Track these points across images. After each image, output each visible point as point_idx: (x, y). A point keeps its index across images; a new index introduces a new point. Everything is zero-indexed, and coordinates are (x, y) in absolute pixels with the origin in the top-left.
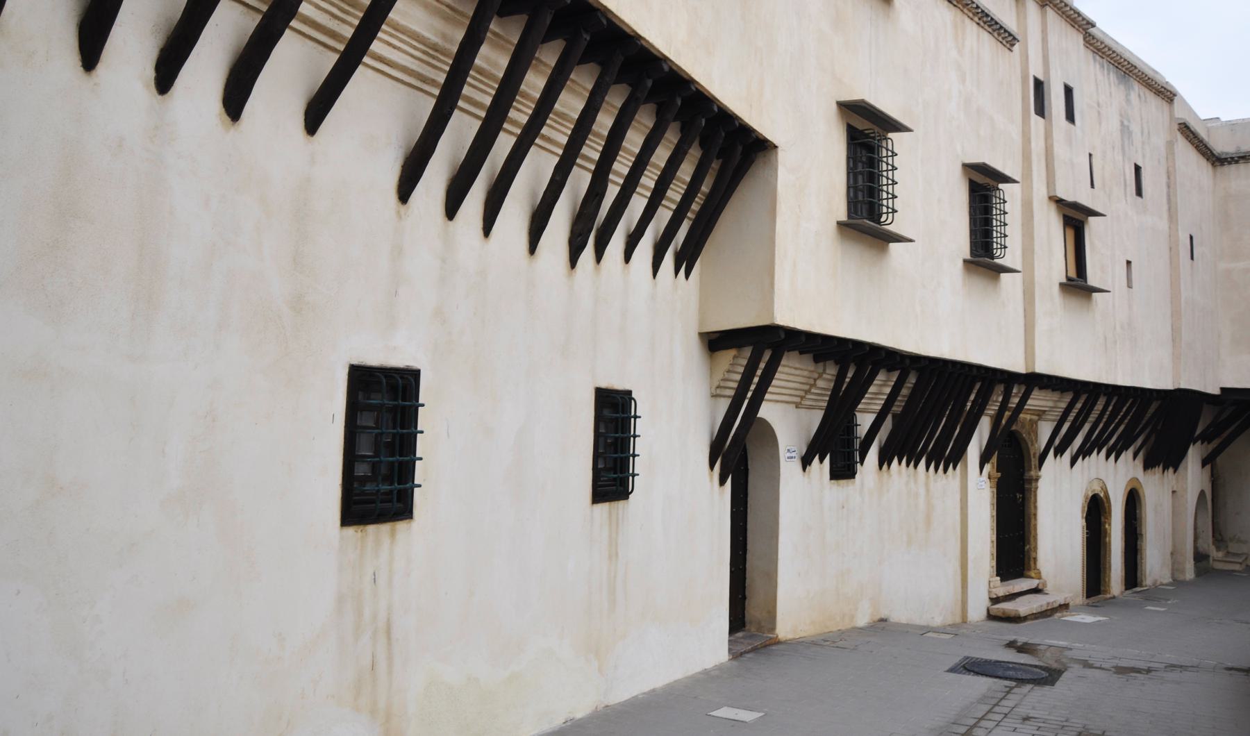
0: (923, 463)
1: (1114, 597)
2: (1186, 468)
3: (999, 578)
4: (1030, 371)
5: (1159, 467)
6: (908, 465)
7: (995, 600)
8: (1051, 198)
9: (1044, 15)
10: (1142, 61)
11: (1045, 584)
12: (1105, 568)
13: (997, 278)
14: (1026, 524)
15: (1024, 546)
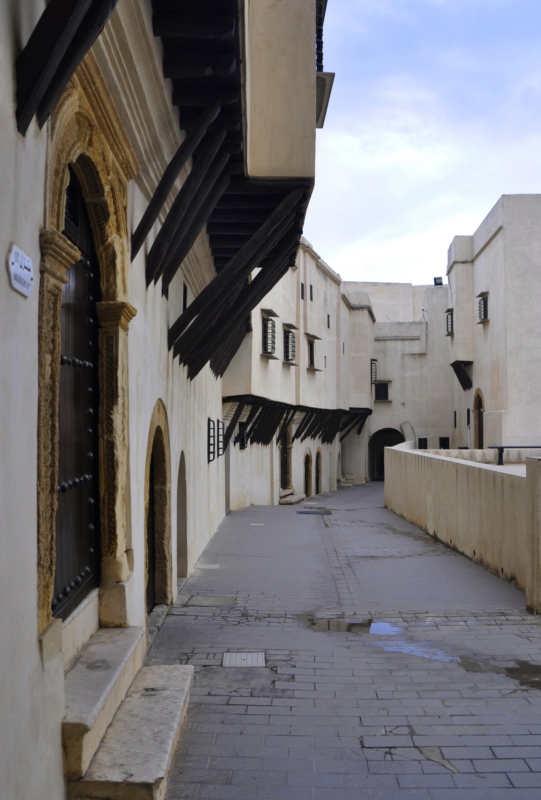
0: (261, 443)
1: (313, 498)
2: (335, 443)
3: (282, 489)
4: (298, 405)
6: (257, 444)
8: (305, 333)
9: (305, 256)
10: (332, 269)
12: (310, 485)
15: (287, 476)
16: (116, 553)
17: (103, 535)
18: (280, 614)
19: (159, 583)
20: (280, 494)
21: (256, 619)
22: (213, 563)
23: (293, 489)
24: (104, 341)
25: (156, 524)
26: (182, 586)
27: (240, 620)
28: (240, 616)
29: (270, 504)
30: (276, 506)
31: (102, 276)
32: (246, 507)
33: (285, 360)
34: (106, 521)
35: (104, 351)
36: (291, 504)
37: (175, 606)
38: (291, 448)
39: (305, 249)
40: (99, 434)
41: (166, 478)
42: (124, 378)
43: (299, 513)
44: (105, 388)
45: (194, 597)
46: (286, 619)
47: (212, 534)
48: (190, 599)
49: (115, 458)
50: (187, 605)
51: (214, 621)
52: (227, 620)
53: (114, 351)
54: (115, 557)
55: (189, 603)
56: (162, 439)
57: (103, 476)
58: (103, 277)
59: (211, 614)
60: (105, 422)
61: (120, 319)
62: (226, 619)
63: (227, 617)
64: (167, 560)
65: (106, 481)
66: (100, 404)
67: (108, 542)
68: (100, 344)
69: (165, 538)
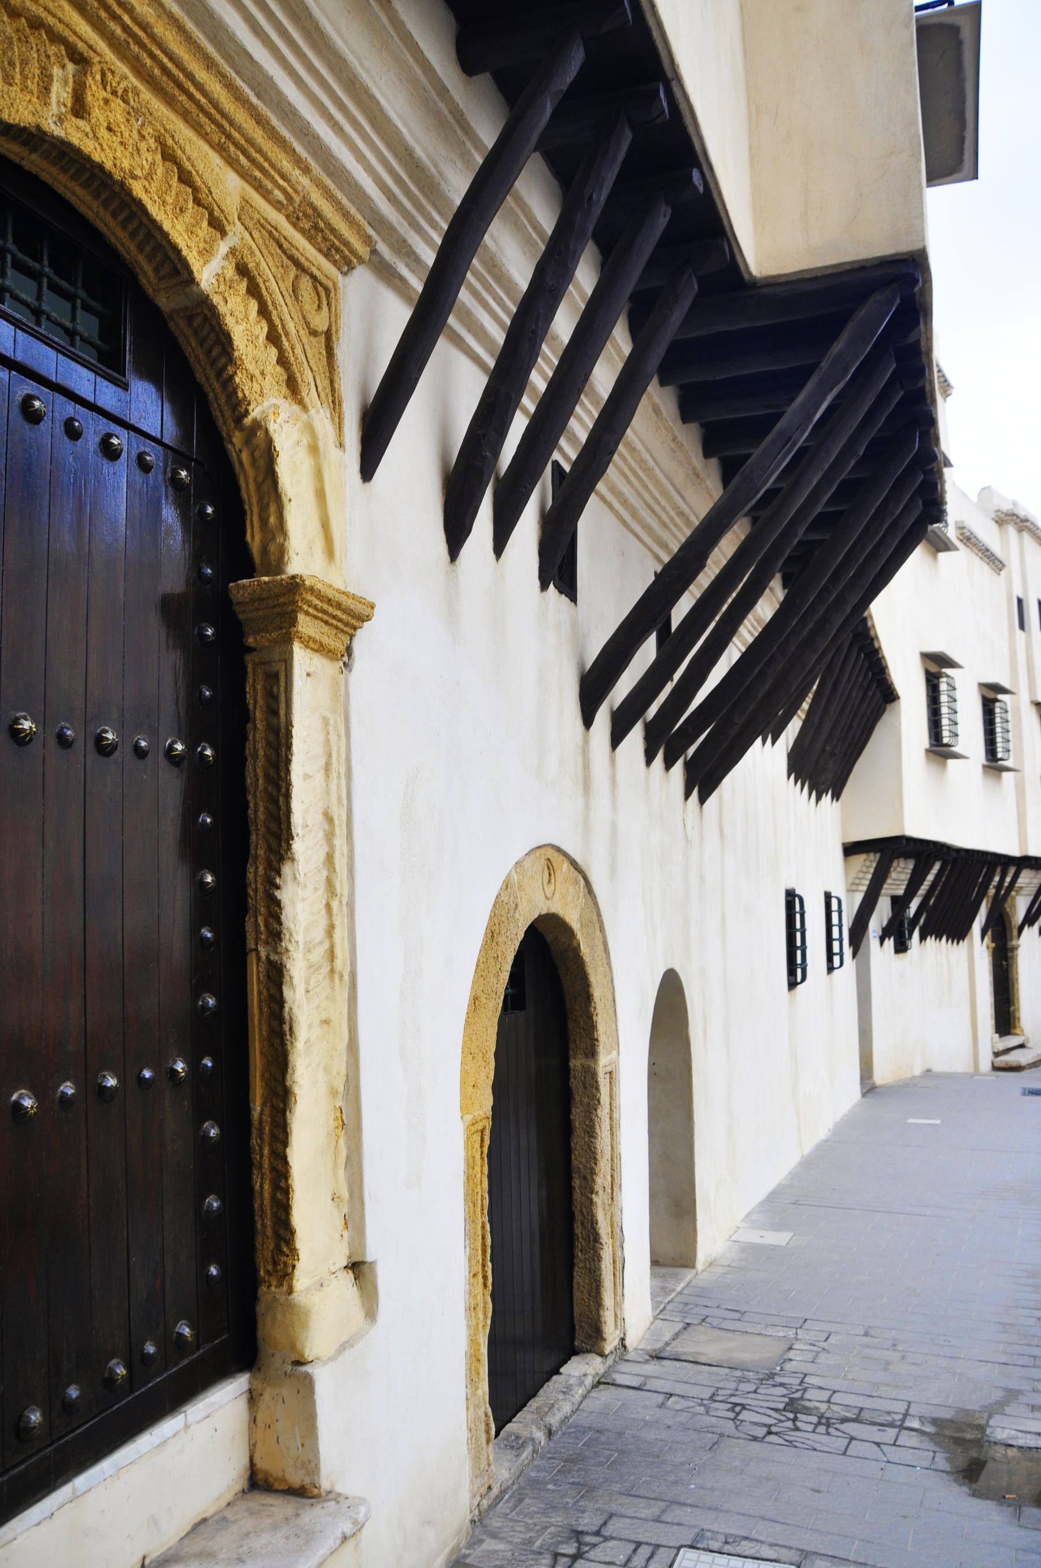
5: (889, 939)
7: (997, 1054)
8: (1032, 702)
9: (1021, 539)
11: (1028, 1040)
13: (999, 777)
14: (1010, 988)
15: (1009, 1007)
16: (292, 1279)
17: (259, 1226)
18: (889, 1413)
19: (583, 1299)
20: (993, 1047)
21: (819, 1423)
22: (777, 1227)
23: (1023, 1035)
24: (259, 687)
25: (576, 1153)
26: (673, 1294)
27: (774, 1421)
28: (781, 1406)
29: (971, 1070)
30: (985, 1075)
31: (248, 513)
32: (914, 1077)
33: (987, 760)
34: (266, 1187)
35: (258, 714)
36: (1016, 1069)
37: (631, 1355)
38: (1014, 949)
39: (1020, 524)
40: (248, 942)
41: (597, 1040)
42: (333, 788)
43: (1030, 1092)
44: (261, 816)
45: (691, 1326)
46: (904, 1432)
47: (808, 1147)
48: (676, 1336)
49: (287, 1009)
50: (662, 1355)
51: (708, 1418)
52: (740, 1417)
53: (282, 712)
54: (290, 1291)
55: (668, 1349)
56: (575, 944)
57: (258, 1059)
58: (252, 515)
59: (707, 1393)
60: (262, 909)
61: (293, 622)
62: (738, 1414)
63: (744, 1407)
64: (601, 1243)
65: (267, 1075)
66: (250, 861)
67: (271, 1246)
68: (248, 696)
69: (598, 1187)
